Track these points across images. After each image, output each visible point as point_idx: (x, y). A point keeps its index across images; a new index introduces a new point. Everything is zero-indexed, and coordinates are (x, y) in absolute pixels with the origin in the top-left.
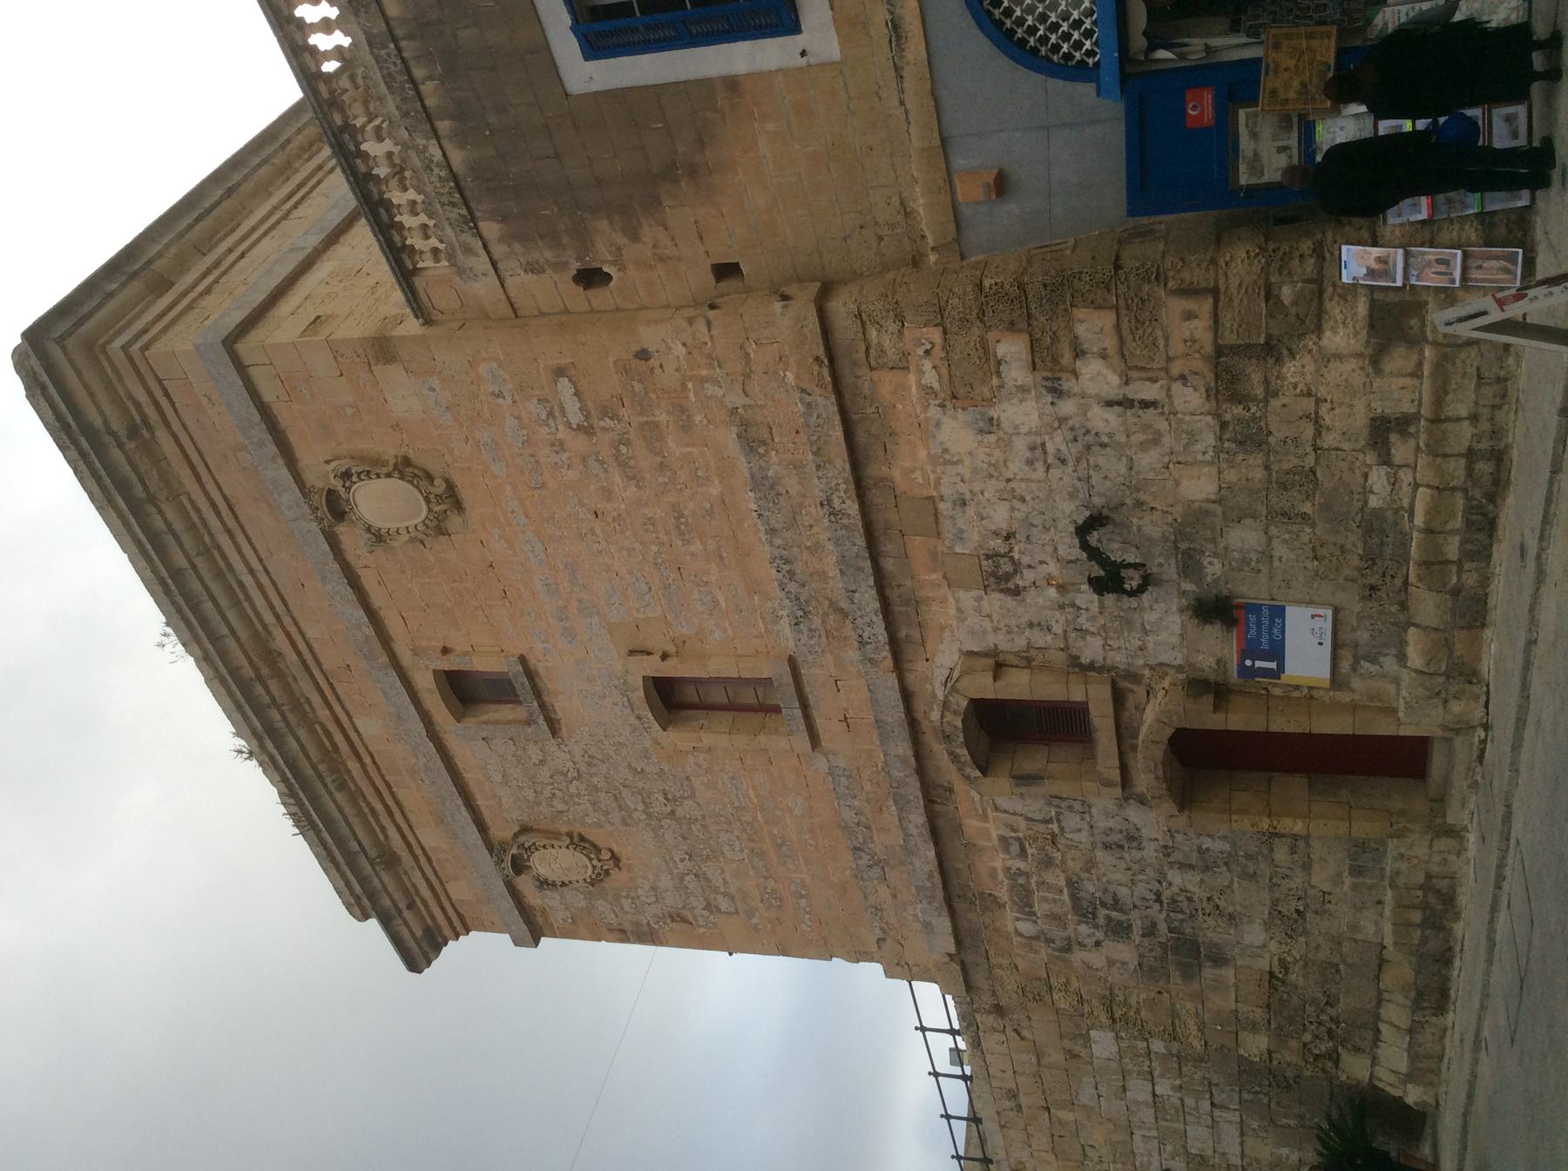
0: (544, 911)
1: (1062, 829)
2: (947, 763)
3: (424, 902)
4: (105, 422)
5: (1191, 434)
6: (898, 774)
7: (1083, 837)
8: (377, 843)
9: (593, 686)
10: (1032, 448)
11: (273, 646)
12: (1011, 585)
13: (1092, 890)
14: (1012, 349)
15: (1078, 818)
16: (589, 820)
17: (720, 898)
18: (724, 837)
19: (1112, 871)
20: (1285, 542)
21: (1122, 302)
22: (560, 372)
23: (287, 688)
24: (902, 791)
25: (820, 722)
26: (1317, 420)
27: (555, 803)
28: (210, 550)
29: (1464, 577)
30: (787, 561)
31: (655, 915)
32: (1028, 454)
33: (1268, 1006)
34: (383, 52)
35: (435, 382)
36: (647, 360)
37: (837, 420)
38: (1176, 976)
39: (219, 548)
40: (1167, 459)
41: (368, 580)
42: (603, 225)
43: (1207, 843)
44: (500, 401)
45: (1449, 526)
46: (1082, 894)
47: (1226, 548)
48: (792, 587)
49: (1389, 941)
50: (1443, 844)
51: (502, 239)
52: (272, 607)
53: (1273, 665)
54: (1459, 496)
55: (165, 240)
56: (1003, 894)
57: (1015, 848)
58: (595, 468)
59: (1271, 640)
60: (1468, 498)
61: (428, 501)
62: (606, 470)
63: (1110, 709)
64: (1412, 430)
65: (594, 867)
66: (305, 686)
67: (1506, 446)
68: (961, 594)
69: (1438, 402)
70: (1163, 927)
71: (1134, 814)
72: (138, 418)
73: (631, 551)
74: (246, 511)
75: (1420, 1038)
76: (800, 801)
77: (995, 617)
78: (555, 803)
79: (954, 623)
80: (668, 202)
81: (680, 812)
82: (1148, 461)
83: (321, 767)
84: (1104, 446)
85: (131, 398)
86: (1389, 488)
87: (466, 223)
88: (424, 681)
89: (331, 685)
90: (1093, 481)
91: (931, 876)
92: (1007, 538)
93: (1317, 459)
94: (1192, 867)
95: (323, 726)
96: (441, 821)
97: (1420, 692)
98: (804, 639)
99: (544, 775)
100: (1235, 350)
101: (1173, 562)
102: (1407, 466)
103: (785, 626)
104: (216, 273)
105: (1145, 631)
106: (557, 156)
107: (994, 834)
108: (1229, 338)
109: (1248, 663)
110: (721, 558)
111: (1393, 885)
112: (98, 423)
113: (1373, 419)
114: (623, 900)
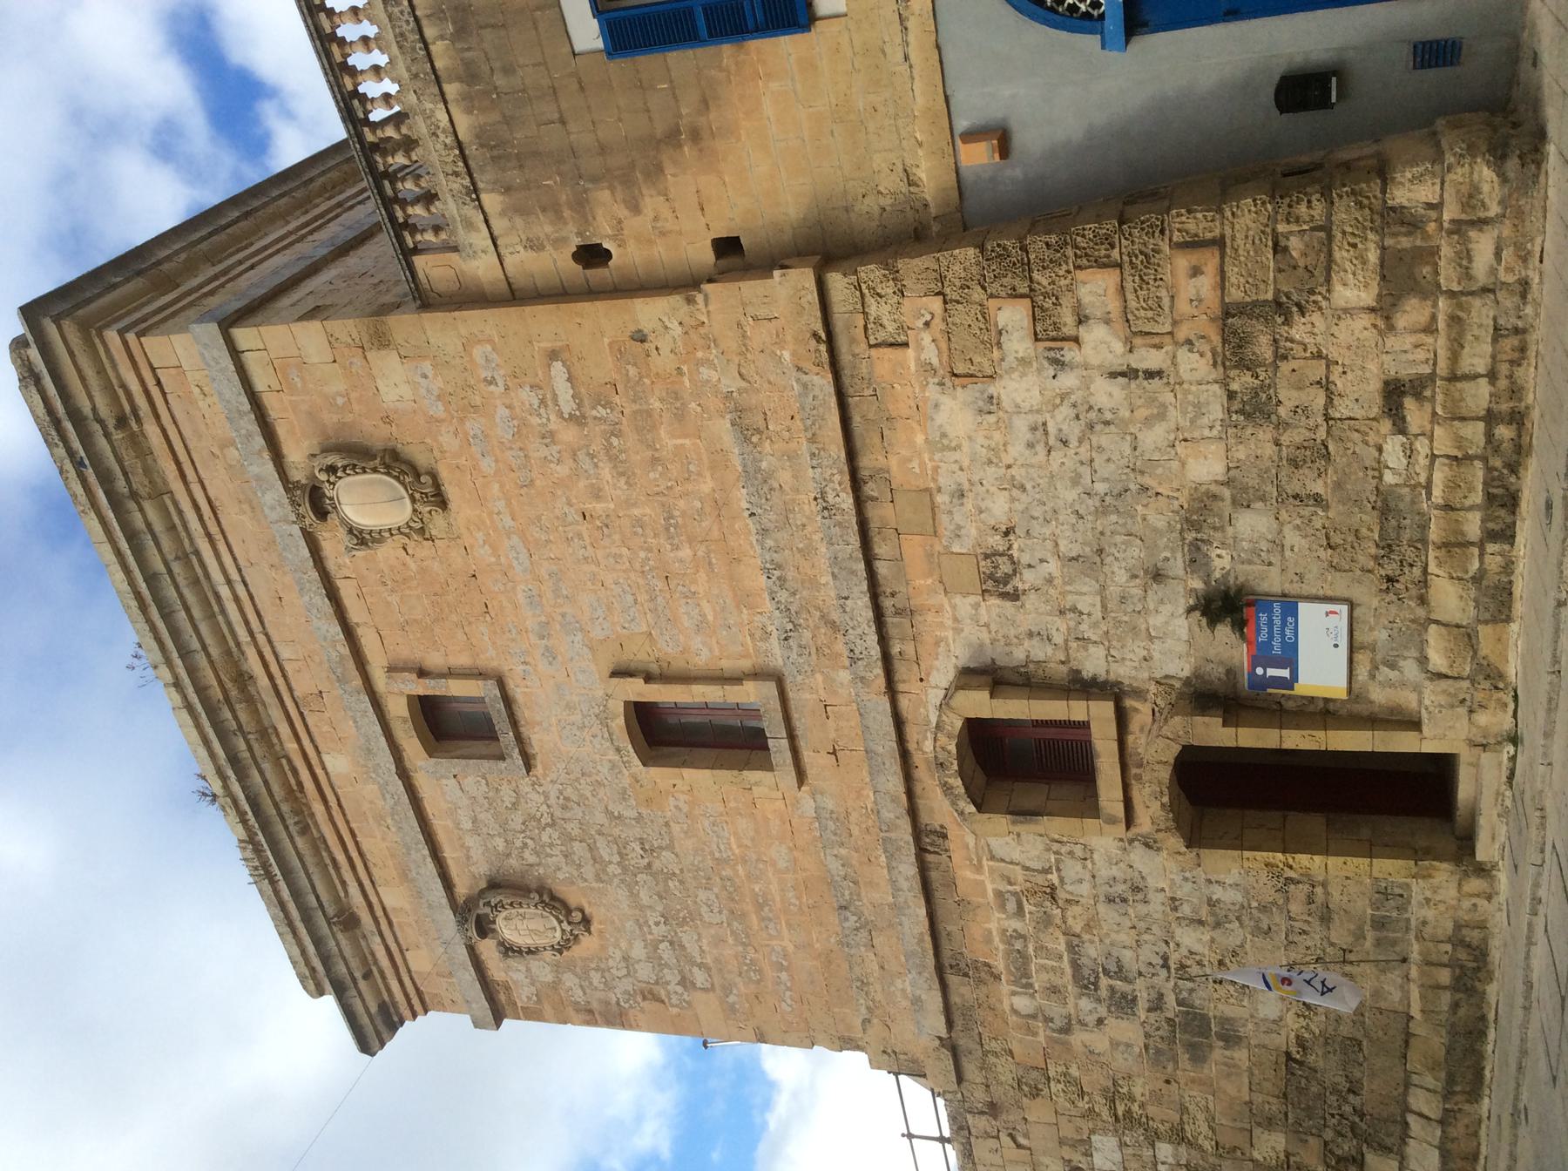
0: (507, 988)
1: (1062, 880)
2: (943, 804)
3: (382, 973)
4: (94, 409)
5: (1198, 405)
6: (887, 815)
7: (1085, 889)
8: (337, 899)
9: (571, 716)
10: (1034, 429)
11: (245, 667)
12: (1009, 588)
13: (1093, 954)
14: (1013, 316)
15: (1079, 867)
16: (561, 876)
17: (695, 970)
18: (702, 895)
19: (1115, 937)
20: (1298, 527)
21: (1126, 258)
22: (553, 355)
23: (255, 712)
24: (893, 835)
25: (807, 756)
26: (1326, 385)
27: (527, 854)
28: (188, 556)
29: (1488, 559)
30: (779, 567)
31: (626, 992)
32: (1029, 436)
33: (1285, 1096)
34: (396, 10)
35: (427, 366)
36: (642, 341)
37: (833, 401)
38: (1184, 1057)
39: (197, 553)
40: (1172, 437)
41: (347, 591)
42: (604, 195)
43: (1218, 893)
44: (492, 387)
45: (1468, 503)
46: (1084, 960)
47: (1235, 538)
48: (783, 596)
49: (1415, 1011)
50: (1475, 884)
51: (503, 213)
52: (247, 623)
53: (1285, 673)
54: (1478, 464)
55: (177, 247)
56: (999, 964)
57: (1011, 906)
58: (586, 463)
59: (1283, 642)
60: (1489, 469)
61: (413, 500)
62: (596, 466)
63: (1112, 731)
64: (1428, 393)
65: (563, 931)
66: (276, 714)
67: (1527, 408)
68: (958, 600)
69: (1455, 357)
70: (1170, 1000)
71: (1139, 858)
72: (127, 408)
73: (617, 557)
74: (230, 515)
75: (1453, 1132)
76: (784, 850)
77: (993, 627)
78: (527, 854)
79: (950, 634)
80: (669, 169)
81: (657, 865)
82: (1153, 438)
83: (285, 808)
84: (1107, 423)
85: (123, 386)
86: (1405, 462)
87: (468, 194)
88: (398, 708)
89: (301, 714)
90: (1096, 464)
91: (921, 941)
92: (1007, 534)
93: (1328, 432)
94: (1201, 922)
95: (290, 761)
96: (404, 876)
97: (1442, 699)
98: (794, 656)
99: (516, 820)
100: (1243, 310)
101: (1179, 555)
102: (1423, 434)
103: (774, 644)
104: (223, 280)
105: (1151, 638)
106: (563, 122)
107: (990, 888)
108: (1235, 295)
109: (1260, 671)
110: (710, 563)
111: (1420, 937)
112: (86, 407)
113: (1387, 383)
114: (592, 973)
